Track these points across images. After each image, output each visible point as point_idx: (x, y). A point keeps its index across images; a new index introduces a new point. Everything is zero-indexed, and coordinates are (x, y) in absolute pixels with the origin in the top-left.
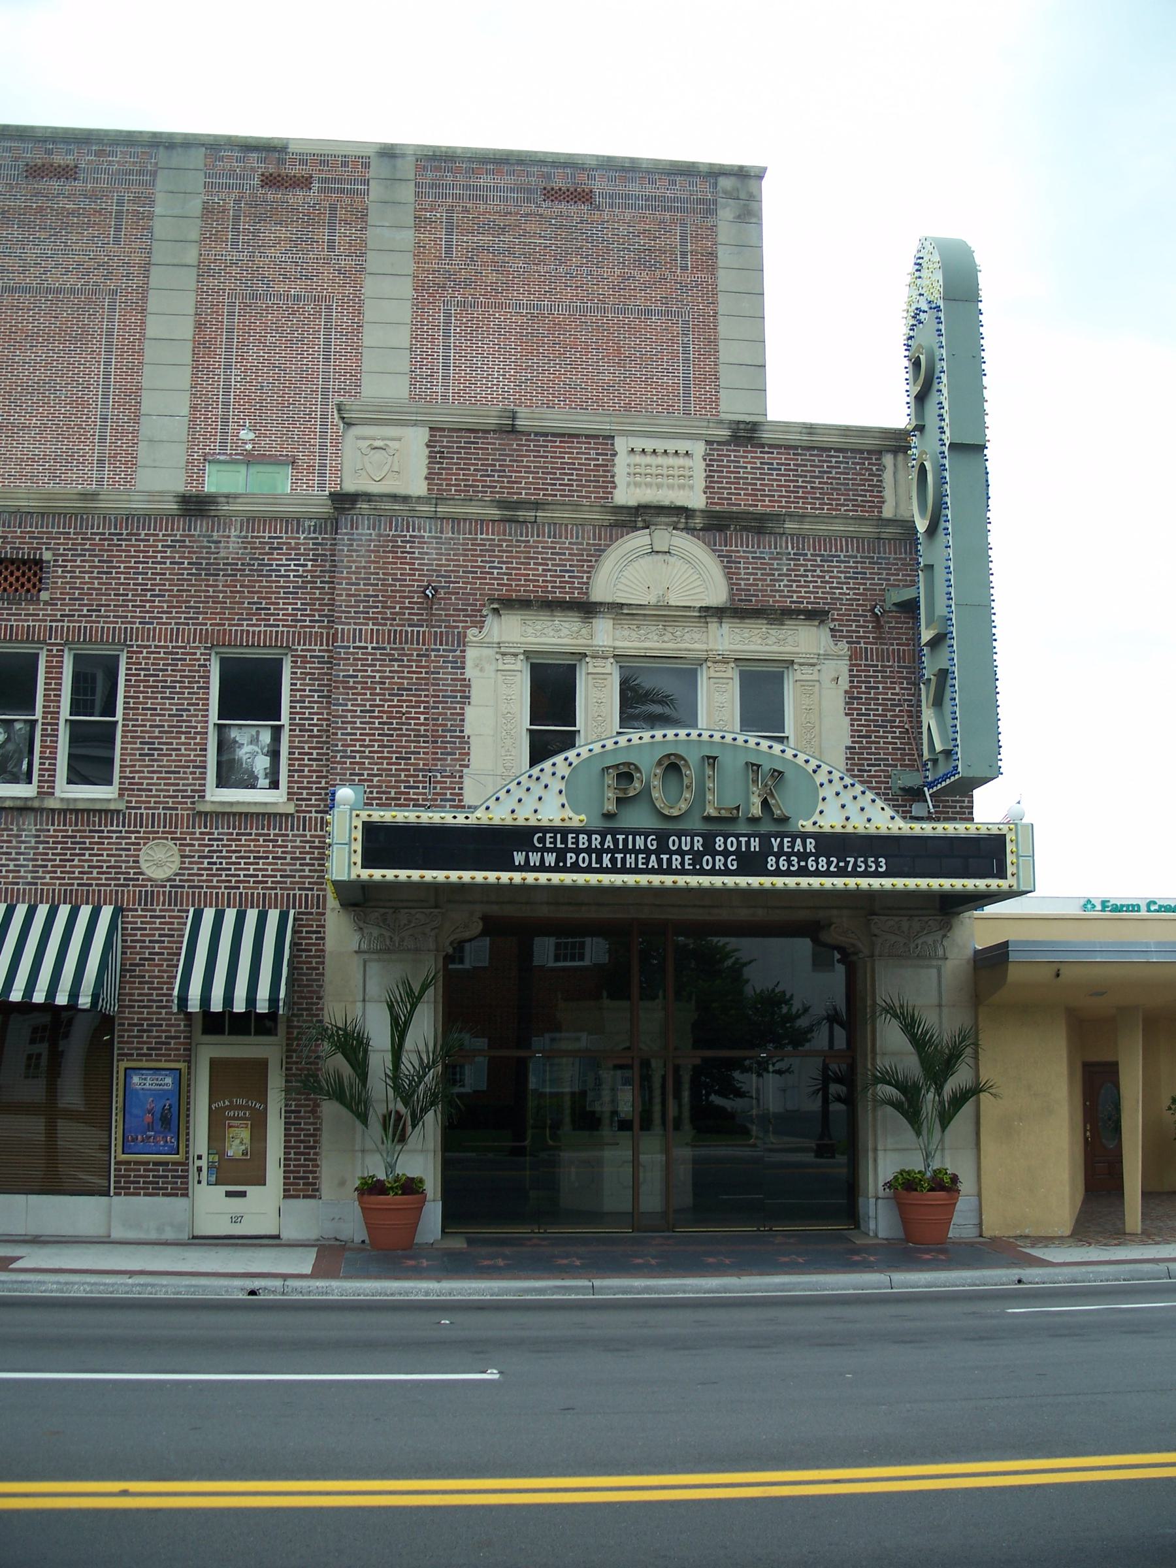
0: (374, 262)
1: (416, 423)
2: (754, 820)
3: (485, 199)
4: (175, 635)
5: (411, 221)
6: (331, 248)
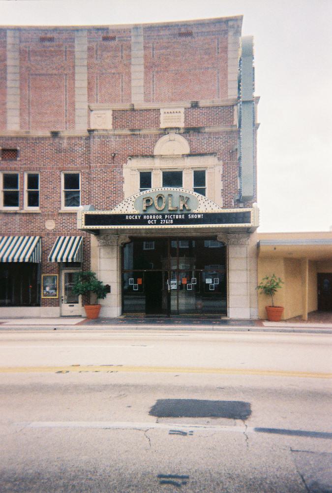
0: (133, 61)
1: (109, 109)
2: (181, 210)
3: (162, 39)
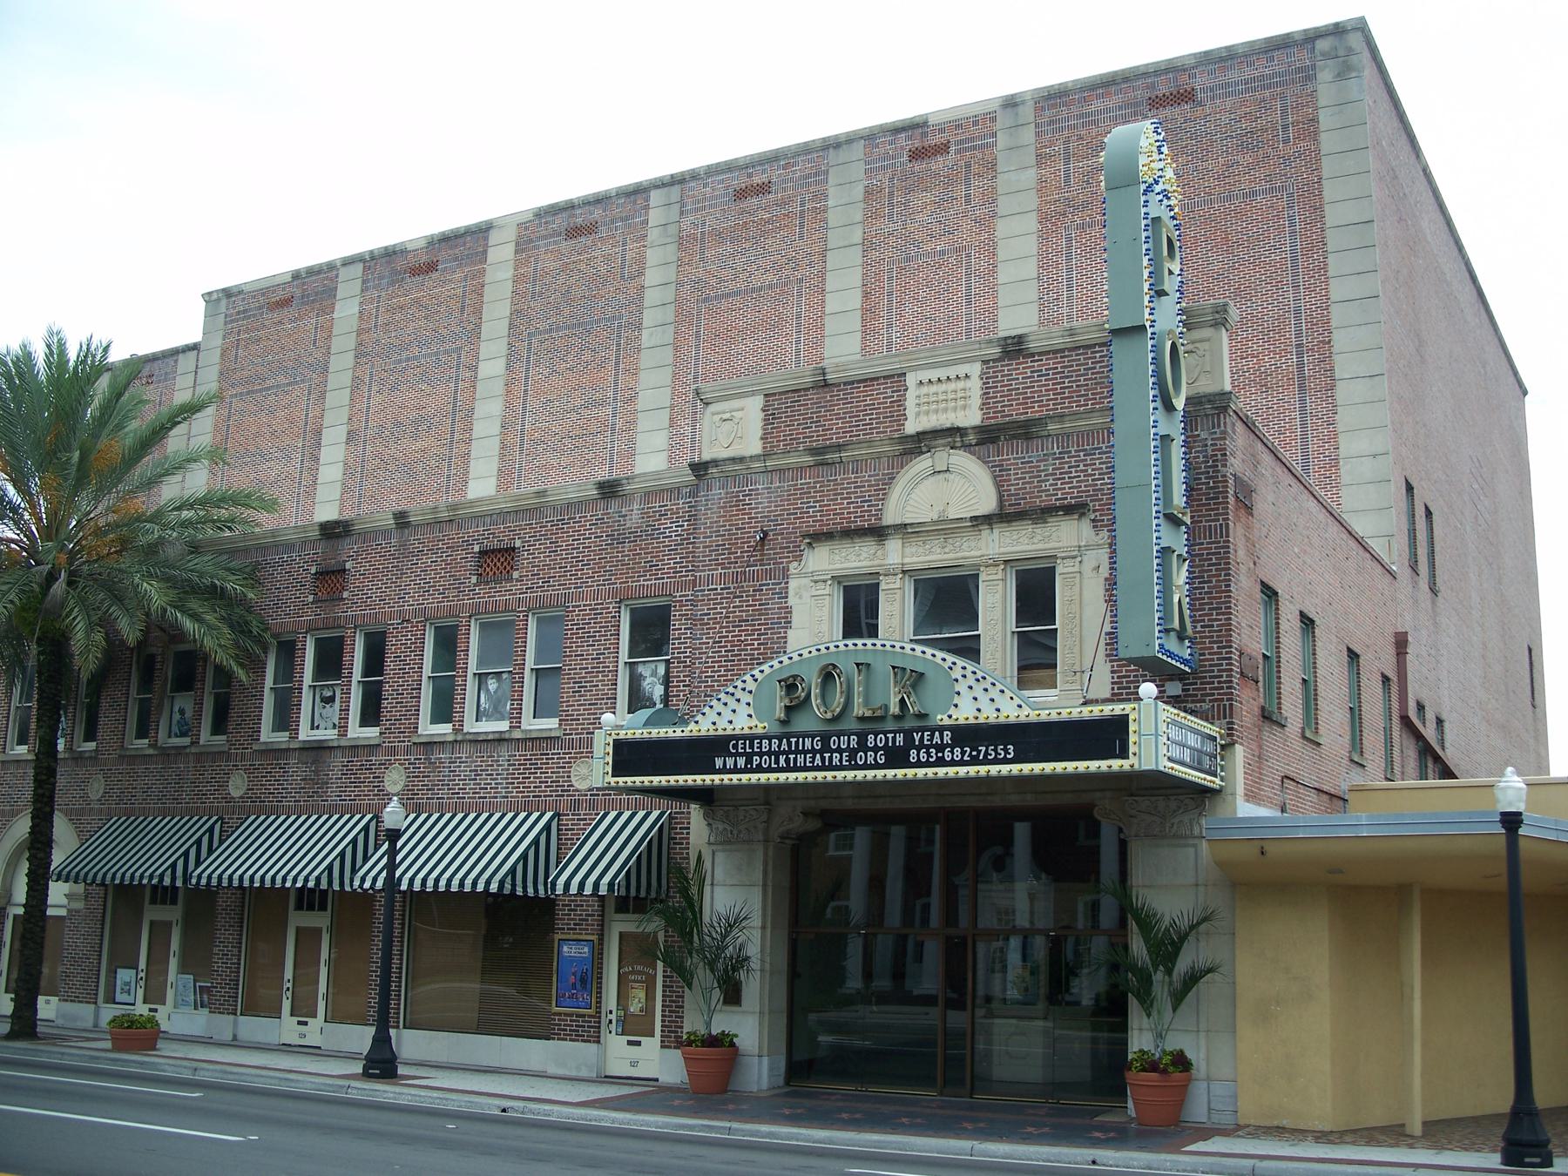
0: (1004, 205)
1: (753, 393)
2: (897, 718)
6: (968, 202)
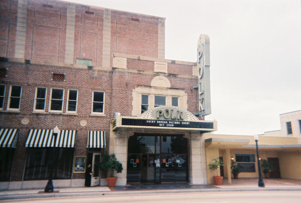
0: (104, 28)
2: (178, 119)
4: (87, 88)
5: (110, 22)
6: (97, 25)
